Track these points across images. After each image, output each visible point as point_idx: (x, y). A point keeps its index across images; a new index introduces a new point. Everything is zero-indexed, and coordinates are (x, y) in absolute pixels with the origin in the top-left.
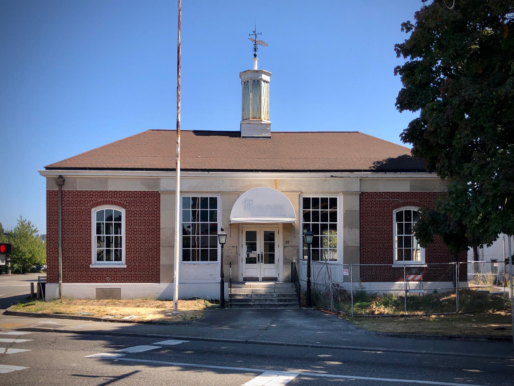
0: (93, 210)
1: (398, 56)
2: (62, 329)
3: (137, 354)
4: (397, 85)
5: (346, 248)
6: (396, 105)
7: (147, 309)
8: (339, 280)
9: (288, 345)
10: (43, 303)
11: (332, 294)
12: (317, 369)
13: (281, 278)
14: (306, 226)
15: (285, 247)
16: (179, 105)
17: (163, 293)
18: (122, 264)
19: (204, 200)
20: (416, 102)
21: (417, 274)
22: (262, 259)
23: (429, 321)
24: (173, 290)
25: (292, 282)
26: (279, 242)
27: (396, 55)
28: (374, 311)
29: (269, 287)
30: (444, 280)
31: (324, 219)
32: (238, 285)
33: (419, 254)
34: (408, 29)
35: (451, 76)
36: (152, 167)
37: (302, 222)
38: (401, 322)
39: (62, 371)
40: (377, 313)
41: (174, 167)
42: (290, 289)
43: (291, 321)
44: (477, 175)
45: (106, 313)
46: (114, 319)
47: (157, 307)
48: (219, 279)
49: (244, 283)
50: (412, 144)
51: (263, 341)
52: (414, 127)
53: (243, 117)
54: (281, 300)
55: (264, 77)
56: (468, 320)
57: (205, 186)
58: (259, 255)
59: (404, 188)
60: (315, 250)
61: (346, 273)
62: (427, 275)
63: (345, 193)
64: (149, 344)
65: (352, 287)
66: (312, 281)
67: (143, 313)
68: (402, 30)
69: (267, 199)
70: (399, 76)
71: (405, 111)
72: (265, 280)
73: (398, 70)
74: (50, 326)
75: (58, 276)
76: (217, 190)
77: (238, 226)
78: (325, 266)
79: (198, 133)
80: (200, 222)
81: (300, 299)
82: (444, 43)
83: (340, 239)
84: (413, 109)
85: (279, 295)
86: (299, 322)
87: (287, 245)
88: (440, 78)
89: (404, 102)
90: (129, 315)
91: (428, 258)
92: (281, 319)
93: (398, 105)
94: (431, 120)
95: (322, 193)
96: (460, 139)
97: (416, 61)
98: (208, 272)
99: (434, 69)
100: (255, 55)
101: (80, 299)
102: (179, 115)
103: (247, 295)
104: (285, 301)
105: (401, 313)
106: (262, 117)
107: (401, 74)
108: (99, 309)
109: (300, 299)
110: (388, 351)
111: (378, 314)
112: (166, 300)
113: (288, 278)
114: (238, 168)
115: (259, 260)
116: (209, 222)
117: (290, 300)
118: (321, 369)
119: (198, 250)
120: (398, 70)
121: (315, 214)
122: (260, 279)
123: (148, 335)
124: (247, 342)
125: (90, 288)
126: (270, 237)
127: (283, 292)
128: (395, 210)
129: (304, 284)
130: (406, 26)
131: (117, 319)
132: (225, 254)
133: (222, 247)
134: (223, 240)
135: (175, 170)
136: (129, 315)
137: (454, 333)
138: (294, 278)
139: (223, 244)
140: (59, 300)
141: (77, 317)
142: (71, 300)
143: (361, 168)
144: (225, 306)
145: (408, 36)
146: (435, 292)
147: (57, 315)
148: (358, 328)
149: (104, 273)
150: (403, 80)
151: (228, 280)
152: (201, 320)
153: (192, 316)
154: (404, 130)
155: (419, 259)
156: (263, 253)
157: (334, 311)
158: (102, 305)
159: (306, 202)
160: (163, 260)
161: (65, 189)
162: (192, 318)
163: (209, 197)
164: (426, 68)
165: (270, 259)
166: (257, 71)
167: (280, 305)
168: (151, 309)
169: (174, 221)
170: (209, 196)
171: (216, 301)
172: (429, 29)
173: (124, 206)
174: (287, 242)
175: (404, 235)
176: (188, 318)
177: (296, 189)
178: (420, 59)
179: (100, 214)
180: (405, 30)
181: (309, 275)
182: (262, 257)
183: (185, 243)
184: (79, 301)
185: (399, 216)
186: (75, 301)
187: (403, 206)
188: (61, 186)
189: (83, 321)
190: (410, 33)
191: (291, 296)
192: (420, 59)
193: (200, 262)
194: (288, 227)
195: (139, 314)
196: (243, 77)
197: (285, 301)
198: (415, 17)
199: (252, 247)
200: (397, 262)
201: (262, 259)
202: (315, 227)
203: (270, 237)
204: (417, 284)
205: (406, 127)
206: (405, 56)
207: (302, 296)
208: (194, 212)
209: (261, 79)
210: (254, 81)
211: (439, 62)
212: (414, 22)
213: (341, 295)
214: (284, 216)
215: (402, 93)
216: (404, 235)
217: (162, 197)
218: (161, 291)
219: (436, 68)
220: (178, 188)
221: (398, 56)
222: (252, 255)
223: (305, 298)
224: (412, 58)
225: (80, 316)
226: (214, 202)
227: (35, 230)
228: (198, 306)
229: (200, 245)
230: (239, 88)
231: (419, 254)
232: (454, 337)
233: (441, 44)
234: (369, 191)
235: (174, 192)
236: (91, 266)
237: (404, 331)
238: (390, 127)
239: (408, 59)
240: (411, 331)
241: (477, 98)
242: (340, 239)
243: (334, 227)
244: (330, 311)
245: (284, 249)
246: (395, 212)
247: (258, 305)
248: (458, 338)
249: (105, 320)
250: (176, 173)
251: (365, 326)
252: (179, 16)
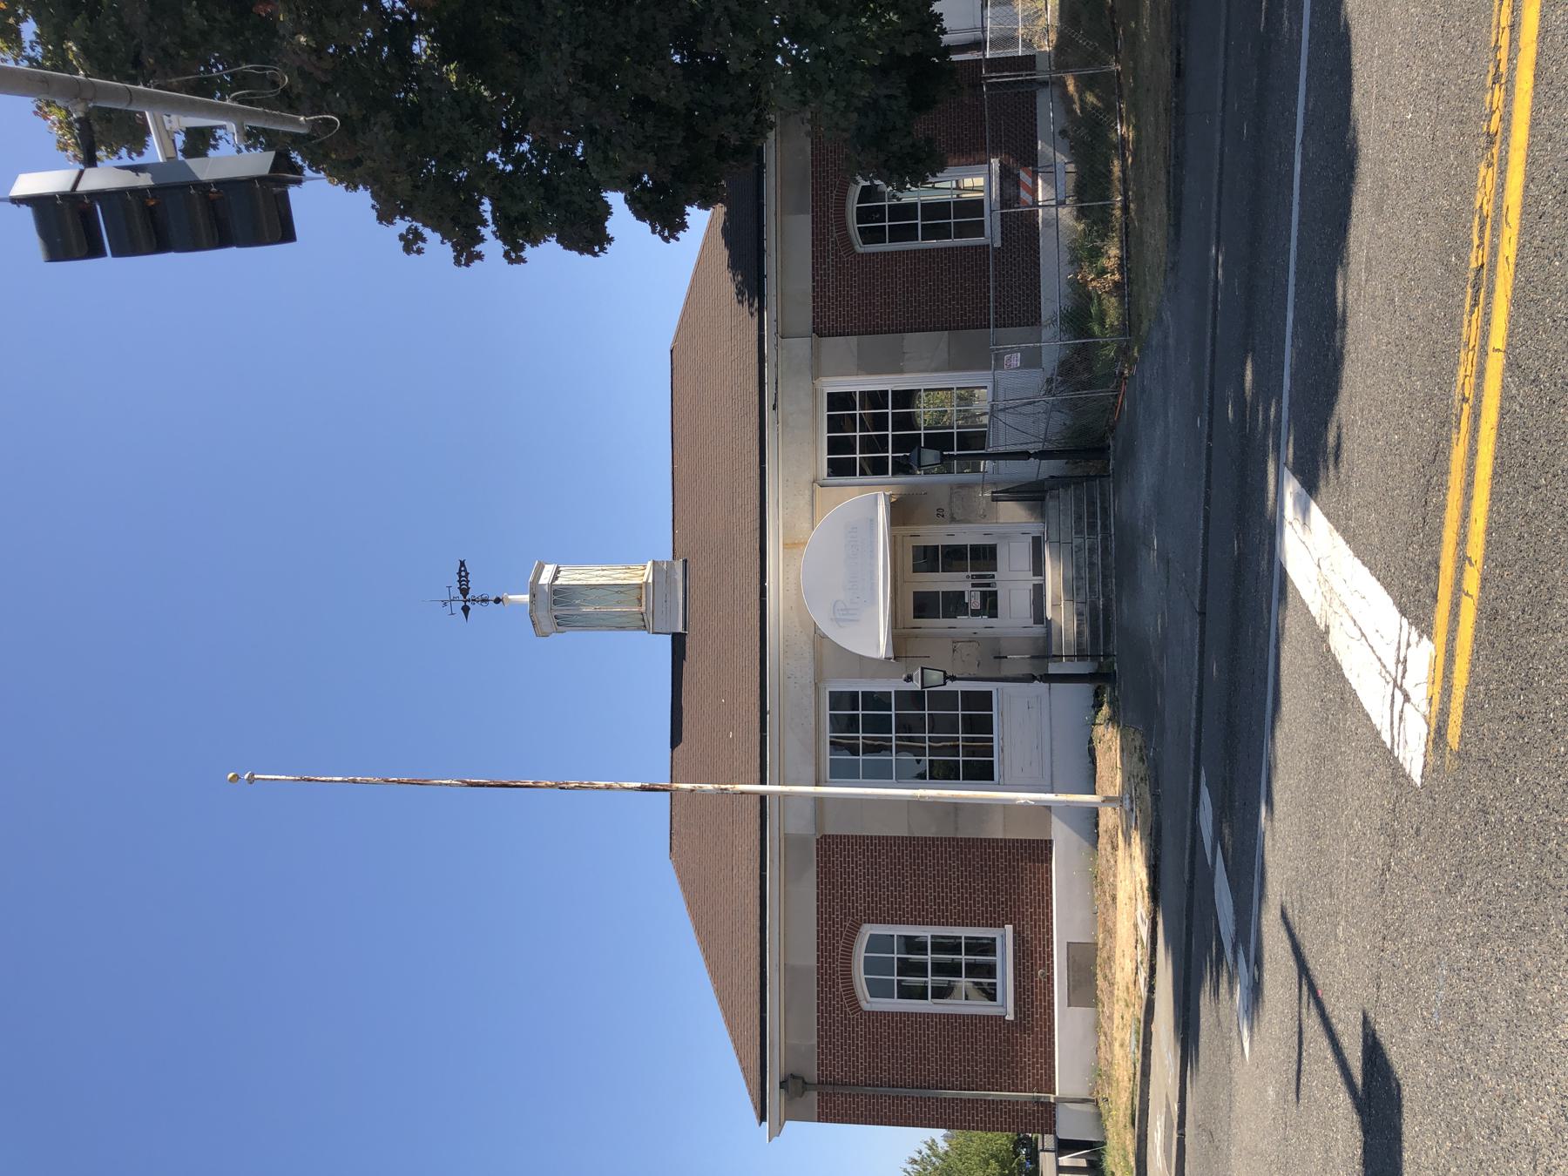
0: (866, 1006)
1: (479, 256)
2: (1176, 1107)
3: (1237, 911)
4: (548, 255)
5: (952, 366)
6: (595, 255)
7: (1121, 877)
8: (1034, 381)
9: (1207, 501)
10: (1108, 1148)
11: (1066, 396)
12: (1266, 417)
13: (1036, 528)
14: (902, 468)
15: (953, 520)
16: (602, 784)
17: (1079, 833)
18: (1003, 937)
19: (844, 724)
20: (589, 205)
21: (1017, 183)
23: (1138, 140)
24: (1068, 806)
25: (1043, 499)
26: (939, 535)
27: (477, 262)
28: (1115, 282)
29: (1056, 557)
31: (880, 422)
32: (1055, 638)
33: (968, 182)
34: (419, 237)
35: (524, 124)
36: (757, 853)
37: (889, 478)
38: (1140, 210)
39: (1290, 1132)
40: (1117, 277)
41: (757, 798)
42: (1062, 505)
43: (1144, 497)
44: (755, 36)
45: (1131, 986)
46: (1146, 965)
47: (1115, 848)
48: (1039, 687)
49: (1049, 622)
50: (688, 209)
51: (1199, 570)
52: (646, 208)
53: (639, 628)
54: (1092, 526)
55: (546, 578)
56: (1133, 38)
57: (801, 723)
58: (974, 585)
59: (802, 227)
60: (962, 446)
61: (1016, 359)
62: (1021, 157)
63: (816, 373)
64: (1211, 876)
65: (1052, 344)
66: (1039, 447)
67: (1130, 889)
68: (419, 251)
69: (834, 568)
70: (529, 252)
71: (608, 231)
72: (1038, 569)
73: (514, 255)
74: (1167, 1137)
75: (1038, 1102)
76: (811, 691)
77: (900, 639)
78: (1001, 416)
79: (676, 739)
80: (893, 735)
81: (1088, 478)
82: (445, 148)
83: (934, 381)
84: (606, 210)
85: (1079, 532)
86: (1146, 477)
87: (947, 514)
88: (530, 151)
89: (588, 235)
90: (1136, 926)
91: (971, 152)
92: (1140, 523)
93: (597, 249)
94: (630, 164)
95: (816, 430)
96: (668, 90)
97: (493, 212)
98: (1021, 716)
99: (509, 168)
100: (498, 601)
101: (1097, 1050)
102: (626, 785)
103: (1079, 614)
104: (1092, 515)
105: (1118, 213)
106: (637, 581)
107: (522, 248)
108: (1122, 1003)
109: (1088, 478)
110: (1218, 233)
111: (1122, 274)
112: (1097, 825)
113: (1032, 509)
114: (758, 638)
115: (988, 585)
116: (893, 713)
117: (1092, 503)
118: (1267, 410)
119: (965, 739)
120: (514, 255)
121: (868, 444)
122: (1037, 580)
123: (1187, 877)
124: (1202, 614)
125: (1066, 1022)
126: (929, 558)
127: (1070, 521)
129: (1049, 468)
130: (411, 242)
131: (1146, 959)
132: (974, 671)
133: (953, 678)
134: (935, 677)
135: (762, 798)
136: (1136, 926)
137: (1167, 64)
138: (1032, 494)
139: (946, 678)
140: (1101, 1104)
141: (1143, 1064)
142: (1100, 1073)
143: (756, 338)
144: (1108, 668)
145: (432, 237)
146: (1063, 133)
147: (1140, 1119)
148: (1160, 321)
150: (535, 242)
151: (1040, 664)
152: (1147, 735)
153: (1135, 759)
154: (654, 232)
155: (979, 181)
157: (1118, 387)
158: (1112, 993)
159: (839, 468)
160: (996, 830)
161: (812, 1074)
162: (1141, 759)
163: (828, 712)
164: (503, 189)
165: (985, 556)
166: (533, 596)
167: (1105, 527)
168: (1120, 865)
169: (898, 797)
170: (827, 712)
171: (1097, 694)
172: (416, 187)
174: (940, 513)
175: (919, 221)
176: (1141, 769)
177: (808, 493)
178: (486, 207)
179: (877, 990)
180: (421, 244)
181: (1025, 455)
183: (945, 773)
184: (1102, 1054)
185: (871, 236)
186: (1103, 1062)
187: (845, 228)
188: (805, 1085)
189: (1153, 1048)
190: (427, 232)
191: (1078, 500)
192: (486, 207)
193: (995, 736)
194: (900, 512)
195: (1133, 899)
196: (546, 630)
197: (1092, 515)
198: (391, 223)
199: (954, 604)
200: (992, 235)
202: (900, 444)
203: (929, 558)
204: (1044, 181)
205: (645, 227)
206: (482, 239)
207: (1078, 472)
208: (869, 749)
209: (551, 585)
210: (555, 602)
211: (490, 156)
212: (401, 225)
213: (1077, 370)
214: (873, 522)
215: (568, 242)
216: (919, 221)
217: (830, 831)
218: (1075, 837)
219: (505, 164)
220: (802, 790)
221: (479, 256)
223: (1083, 465)
224: (484, 223)
225: (1139, 1055)
226: (837, 699)
227: (930, 1148)
228: (1109, 743)
229: (957, 737)
230: (572, 638)
231: (968, 182)
232: (1178, 65)
233: (450, 154)
234: (811, 314)
235: (819, 801)
236: (1010, 1017)
237: (1163, 198)
238: (654, 270)
239: (487, 232)
240: (1163, 178)
241: (573, 55)
242: (934, 381)
243: (905, 398)
245: (959, 522)
246: (861, 248)
247: (1105, 585)
248: (1179, 53)
249: (1151, 989)
250: (772, 793)
251: (1152, 304)
252: (399, 782)
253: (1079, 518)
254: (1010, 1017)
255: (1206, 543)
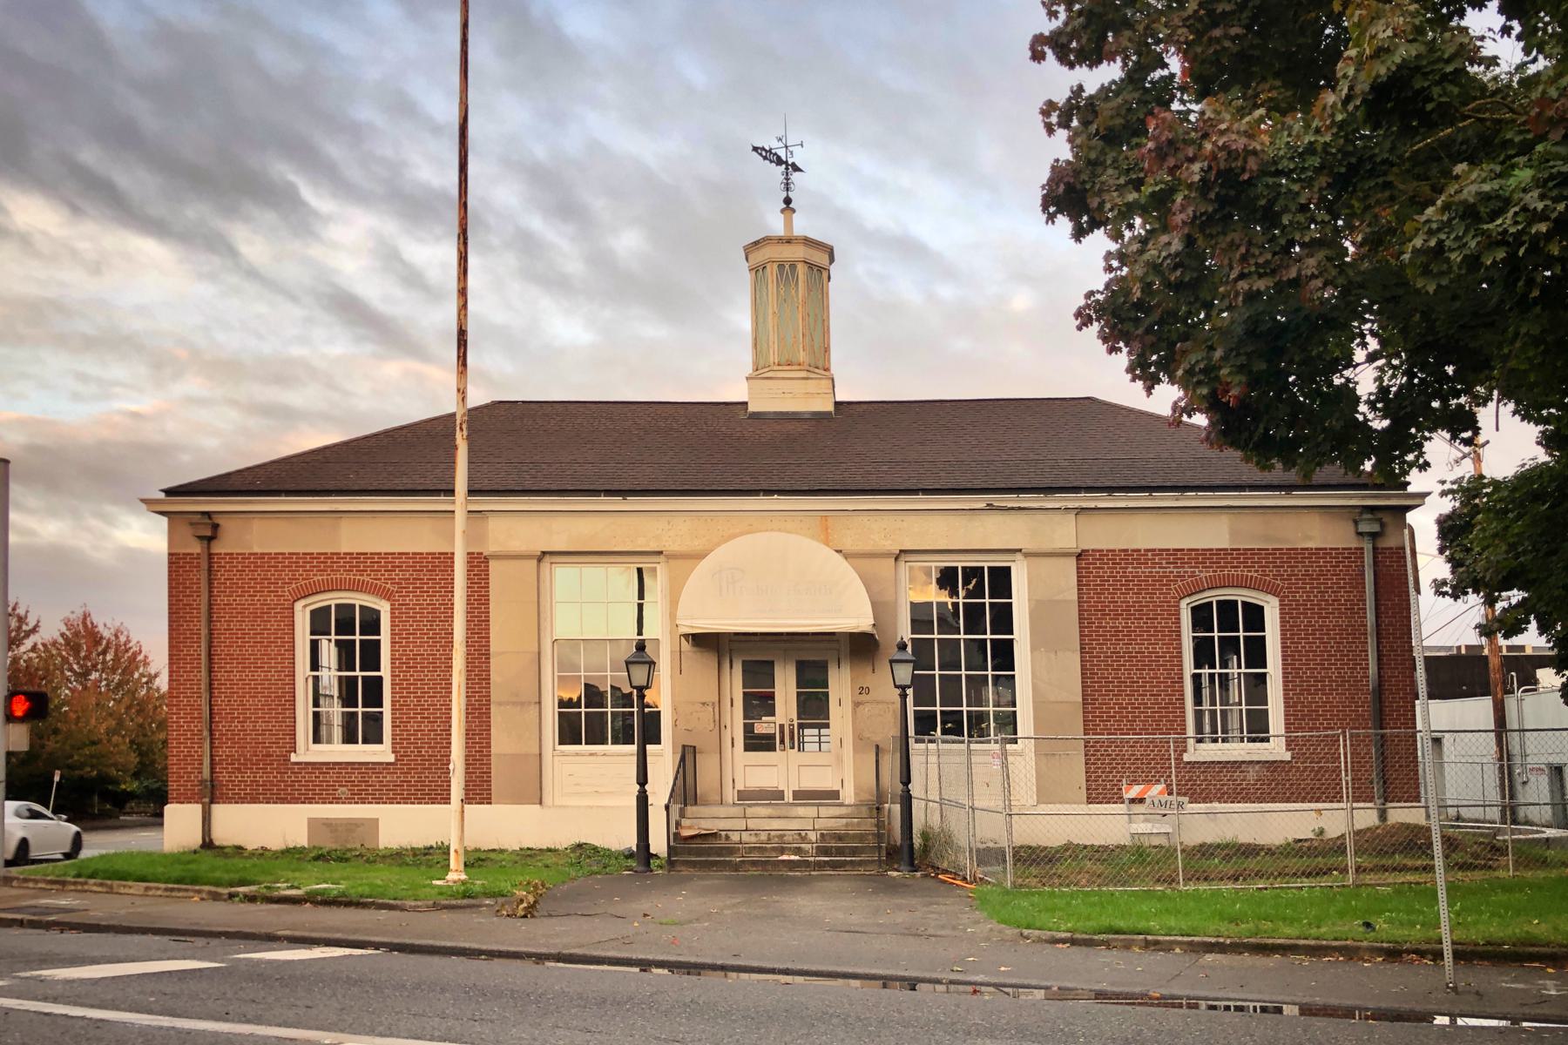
0: (299, 606)
13: (848, 796)
15: (857, 704)
22: (792, 738)
30: (454, 439)
58: (782, 726)
73: (1059, 114)
87: (864, 697)
93: (1052, 209)
115: (782, 741)
128: (1188, 600)
149: (332, 777)
156: (795, 723)
164: (1143, 93)
173: (387, 595)
174: (863, 690)
182: (792, 732)
185: (1201, 616)
191: (861, 838)
201: (792, 738)
222: (761, 728)
236: (294, 758)
244: (964, 879)
247: (754, 863)
253: (840, 838)
254: (294, 758)
255: (786, 972)
